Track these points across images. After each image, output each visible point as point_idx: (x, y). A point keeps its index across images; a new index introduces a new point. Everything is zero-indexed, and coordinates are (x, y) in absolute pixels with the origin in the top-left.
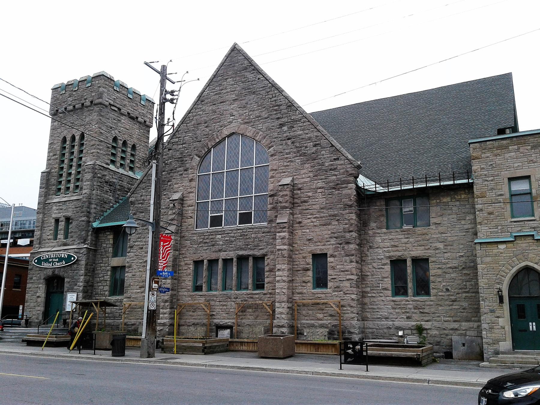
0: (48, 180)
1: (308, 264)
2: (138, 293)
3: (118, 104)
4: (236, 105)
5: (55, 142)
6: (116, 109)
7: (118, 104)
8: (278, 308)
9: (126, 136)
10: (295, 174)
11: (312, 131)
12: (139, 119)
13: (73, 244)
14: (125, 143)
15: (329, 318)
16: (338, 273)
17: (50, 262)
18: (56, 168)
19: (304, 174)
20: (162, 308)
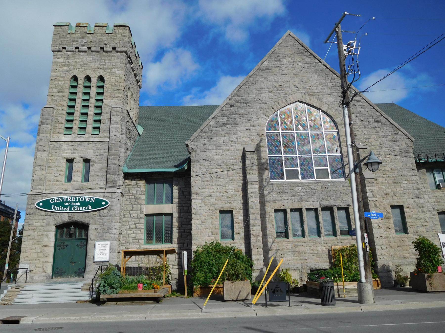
17: (66, 207)
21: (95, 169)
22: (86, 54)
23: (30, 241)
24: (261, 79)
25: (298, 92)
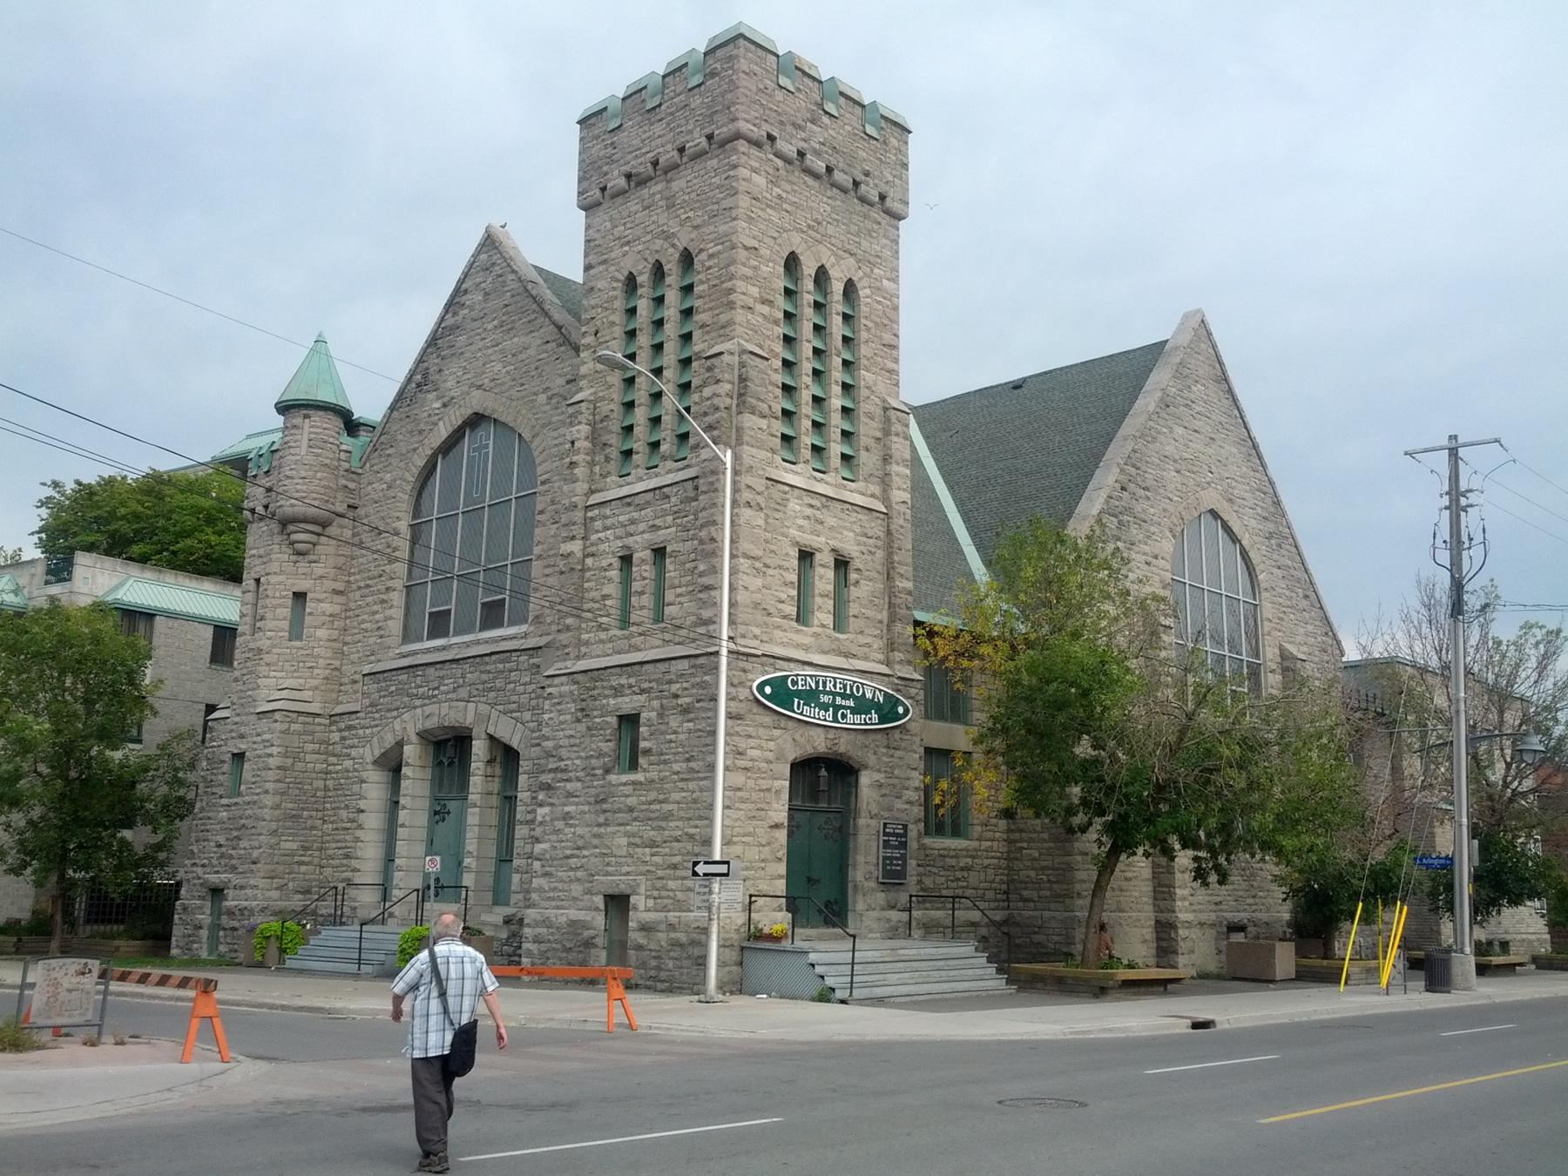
13: (866, 658)
14: (821, 277)
21: (864, 590)
22: (815, 184)
23: (743, 806)
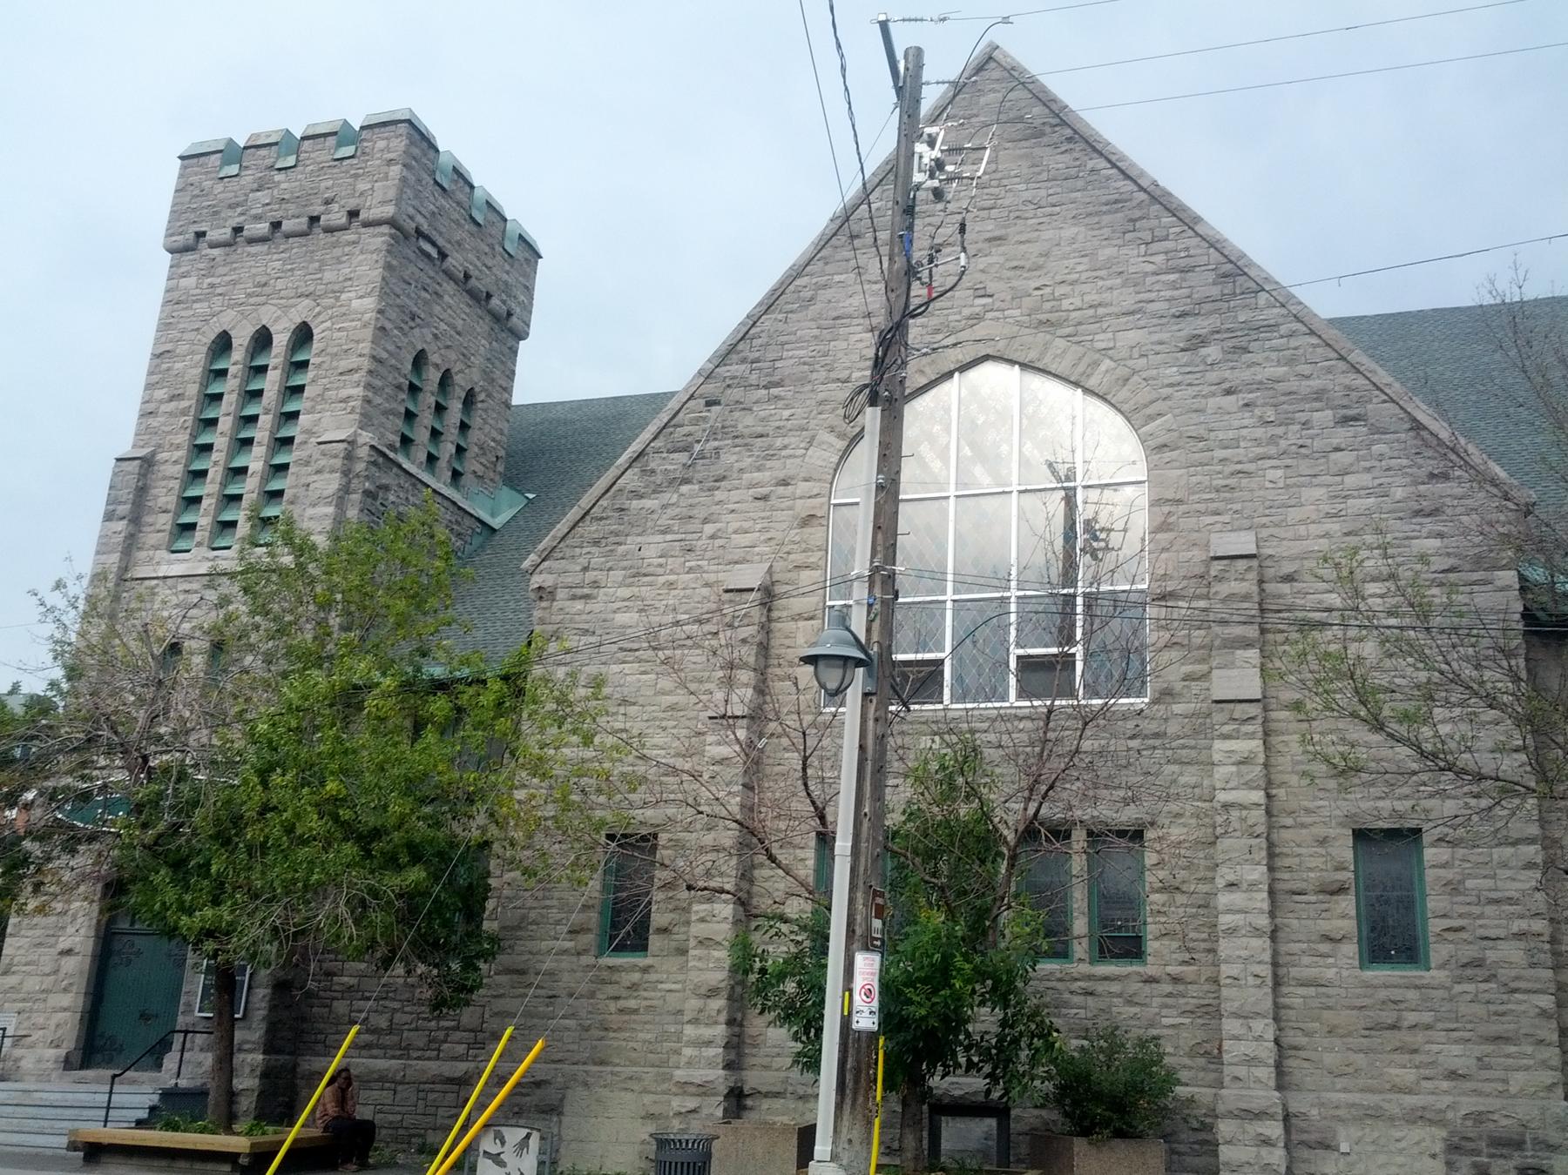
0: (142, 491)
1: (1340, 868)
2: (565, 952)
3: (441, 234)
4: (1001, 260)
5: (182, 348)
6: (434, 253)
7: (441, 234)
8: (1236, 1038)
9: (453, 356)
10: (1265, 520)
11: (1329, 371)
12: (495, 302)
14: (445, 381)
15: (1445, 1085)
16: (1476, 910)
18: (178, 447)
19: (1302, 522)
20: (695, 1022)
24: (837, 278)
25: (990, 315)
